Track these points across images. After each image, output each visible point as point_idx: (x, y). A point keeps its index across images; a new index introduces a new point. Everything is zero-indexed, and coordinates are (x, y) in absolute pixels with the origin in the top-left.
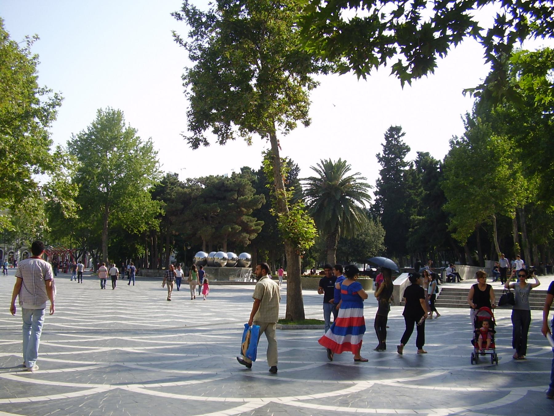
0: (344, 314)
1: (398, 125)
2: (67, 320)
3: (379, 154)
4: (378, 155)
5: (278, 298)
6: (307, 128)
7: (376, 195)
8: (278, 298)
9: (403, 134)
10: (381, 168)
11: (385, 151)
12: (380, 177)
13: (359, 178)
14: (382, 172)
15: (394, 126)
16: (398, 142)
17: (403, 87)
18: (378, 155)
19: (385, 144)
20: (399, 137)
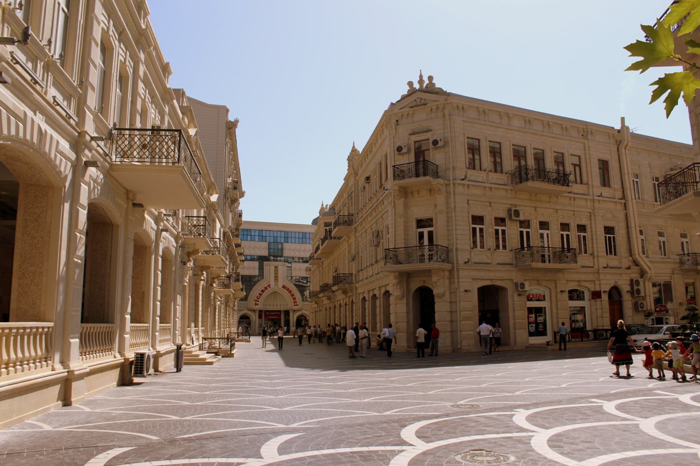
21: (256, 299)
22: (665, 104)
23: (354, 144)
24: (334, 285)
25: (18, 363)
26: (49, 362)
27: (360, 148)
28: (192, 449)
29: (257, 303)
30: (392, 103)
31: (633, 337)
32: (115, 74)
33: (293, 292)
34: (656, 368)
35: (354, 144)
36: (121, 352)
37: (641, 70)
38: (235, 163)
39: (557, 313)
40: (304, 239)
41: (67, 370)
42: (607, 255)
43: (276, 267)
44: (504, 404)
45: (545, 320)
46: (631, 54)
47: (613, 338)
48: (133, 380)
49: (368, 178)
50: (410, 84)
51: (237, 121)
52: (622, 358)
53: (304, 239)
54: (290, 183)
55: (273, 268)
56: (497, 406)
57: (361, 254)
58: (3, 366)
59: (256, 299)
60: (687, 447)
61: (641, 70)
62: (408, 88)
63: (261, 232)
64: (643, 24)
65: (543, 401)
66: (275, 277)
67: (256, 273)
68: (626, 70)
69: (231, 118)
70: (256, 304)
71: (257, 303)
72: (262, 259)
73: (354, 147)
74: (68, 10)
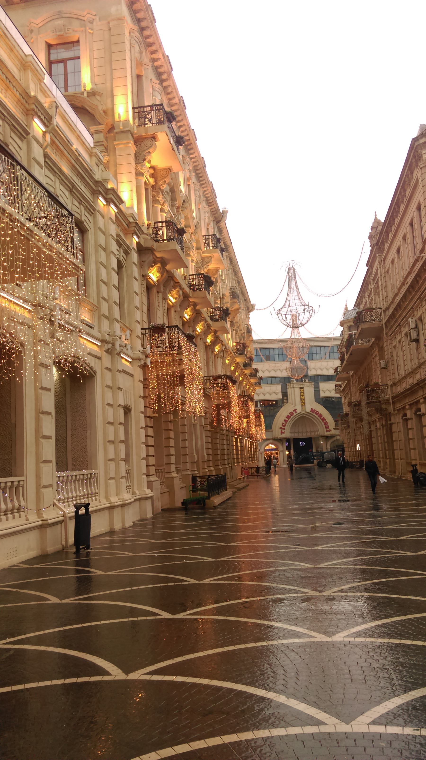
21: (281, 426)
23: (376, 215)
25: (16, 511)
26: (97, 497)
27: (382, 218)
29: (283, 431)
32: (80, 185)
33: (324, 416)
35: (376, 215)
36: (107, 498)
37: (422, 470)
40: (332, 354)
41: (41, 519)
43: (301, 388)
52: (391, 424)
53: (332, 354)
55: (297, 391)
57: (395, 358)
58: (2, 514)
59: (281, 426)
61: (422, 470)
63: (280, 350)
66: (301, 399)
67: (280, 396)
70: (282, 433)
71: (283, 431)
72: (285, 381)
73: (376, 218)
74: (27, 122)
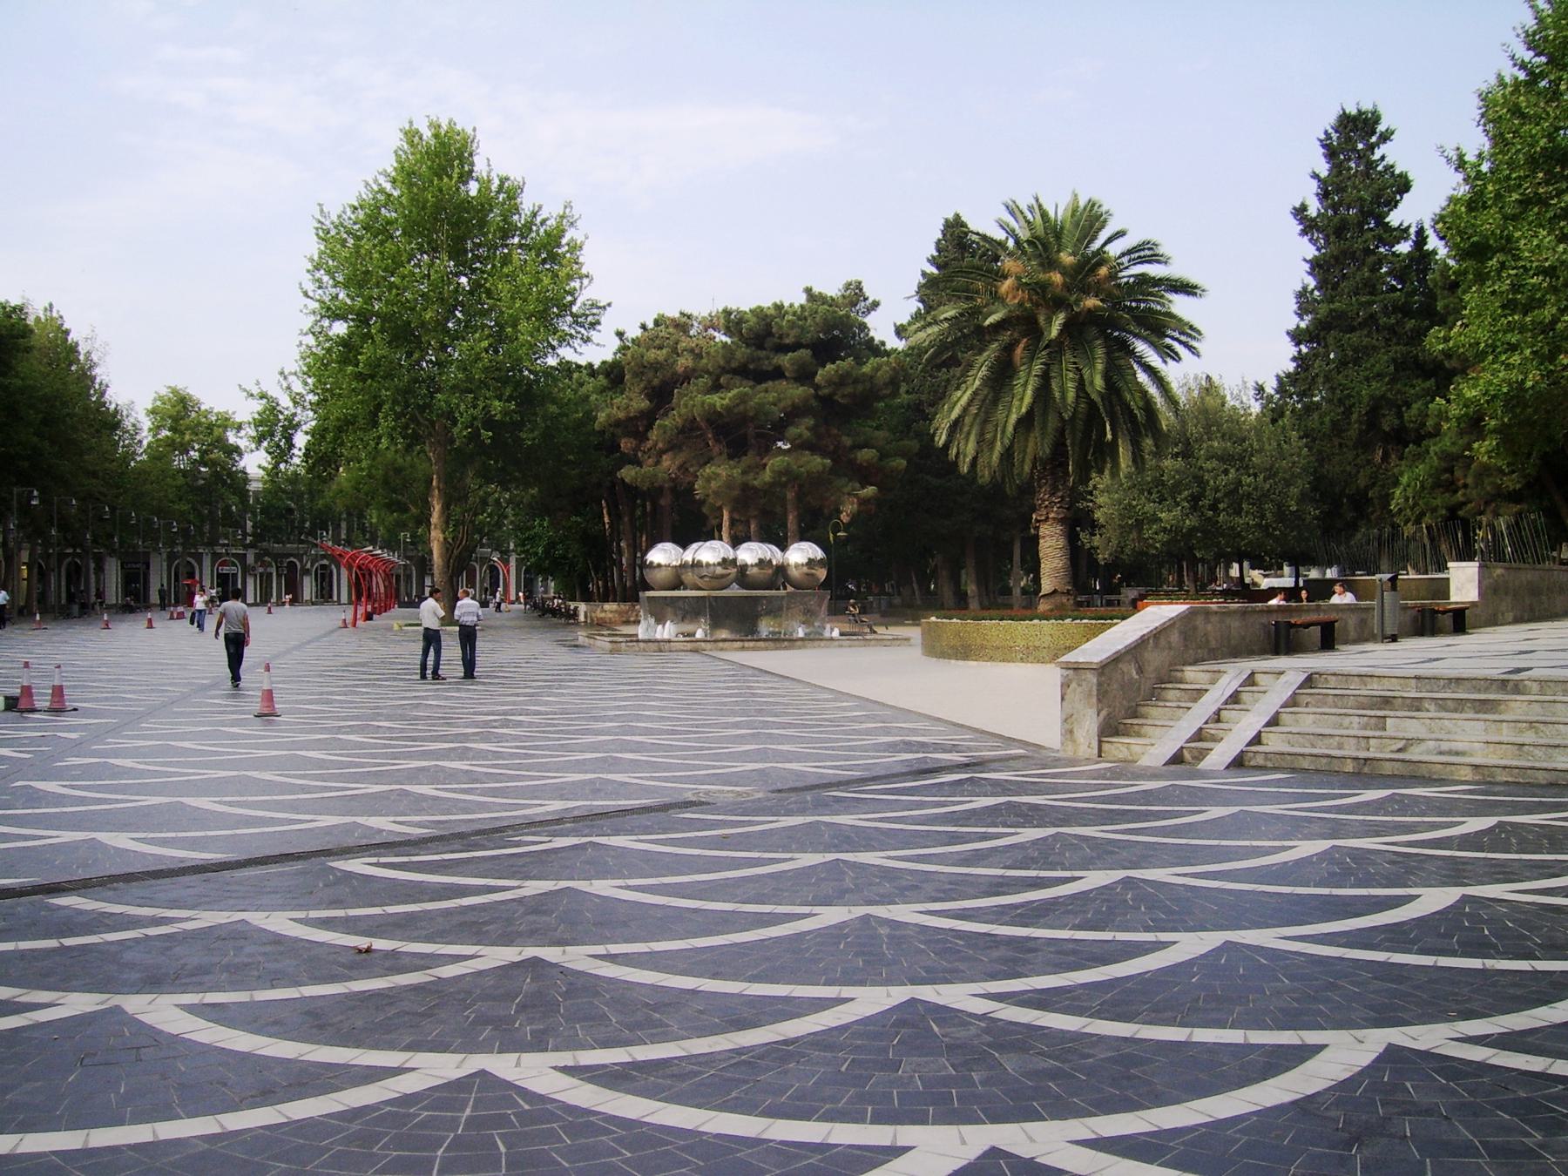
0: (86, 1141)
1: (1367, 106)
2: (887, 873)
3: (1304, 208)
4: (1300, 212)
5: (1216, 667)
6: (853, 278)
7: (1297, 344)
8: (1216, 667)
9: (1386, 137)
10: (1311, 252)
11: (1324, 195)
12: (1312, 283)
13: (1149, 369)
14: (1316, 266)
15: (1352, 110)
16: (1371, 165)
17: (555, 1068)
18: (1300, 212)
19: (1324, 174)
20: (1371, 148)
22: (800, 299)
23: (236, 678)
24: (1333, 582)
28: (135, 976)
30: (1090, 220)
31: (1100, 352)
34: (650, 546)
38: (520, 934)
39: (975, 459)
42: (423, 676)
44: (739, 794)
45: (1460, 621)
46: (1324, 174)
47: (1394, 218)
48: (1209, 407)
49: (26, 665)
50: (1315, 176)
51: (808, 291)
54: (1240, 338)
56: (690, 797)
60: (1185, 875)
62: (1315, 183)
64: (816, 290)
65: (81, 874)
68: (555, 1068)
69: (66, 326)
